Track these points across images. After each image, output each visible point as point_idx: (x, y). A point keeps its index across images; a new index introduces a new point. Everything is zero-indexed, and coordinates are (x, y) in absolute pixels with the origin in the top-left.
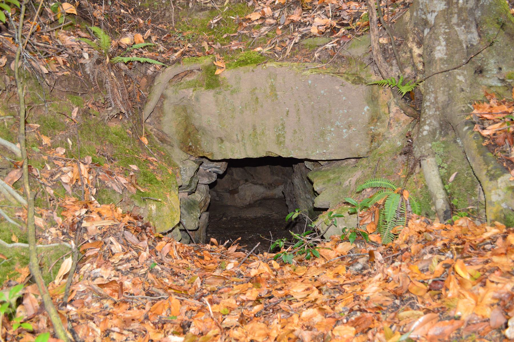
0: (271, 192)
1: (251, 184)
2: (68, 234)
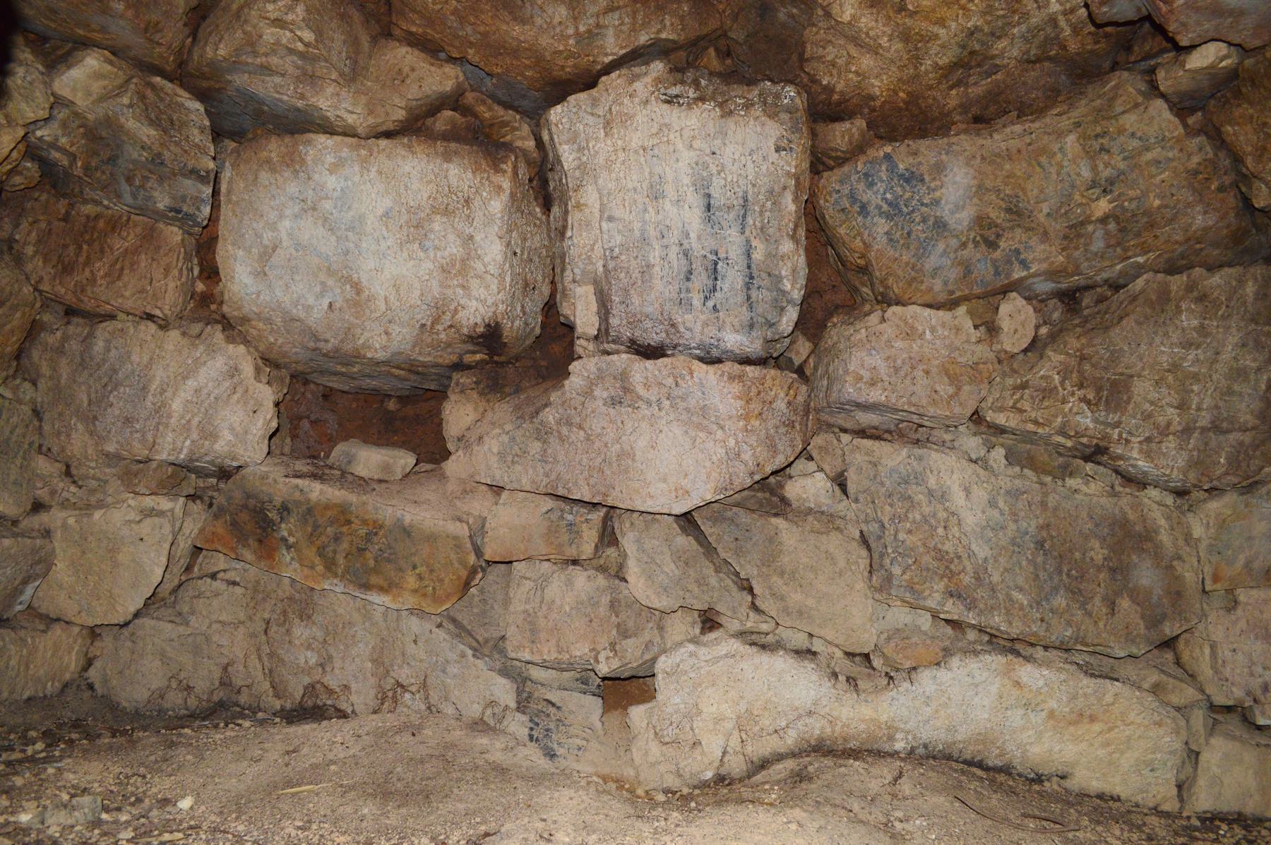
0: (866, 711)
1: (735, 645)
2: (298, 551)
